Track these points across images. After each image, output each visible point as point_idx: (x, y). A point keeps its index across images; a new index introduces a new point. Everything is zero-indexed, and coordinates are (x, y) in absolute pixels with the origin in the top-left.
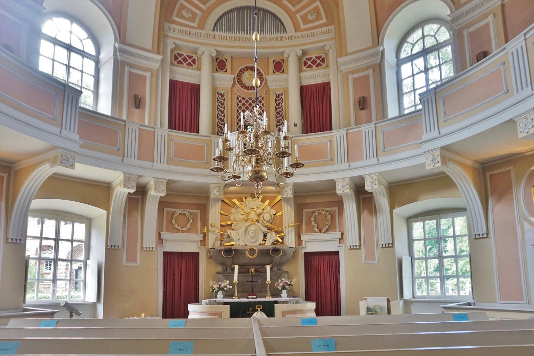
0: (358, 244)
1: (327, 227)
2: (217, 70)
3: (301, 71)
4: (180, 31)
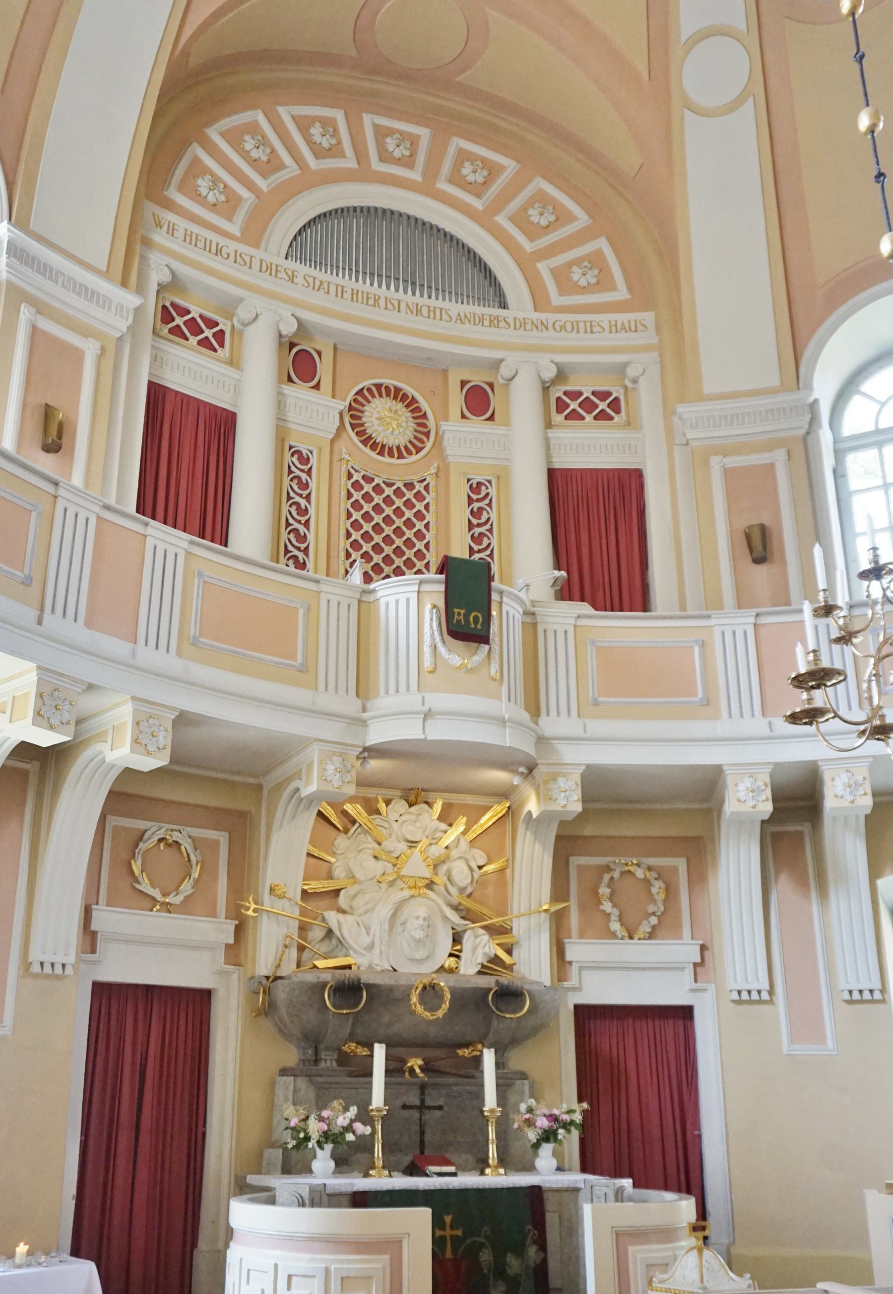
0: (765, 985)
1: (654, 920)
2: (290, 380)
3: (548, 425)
4: (189, 239)
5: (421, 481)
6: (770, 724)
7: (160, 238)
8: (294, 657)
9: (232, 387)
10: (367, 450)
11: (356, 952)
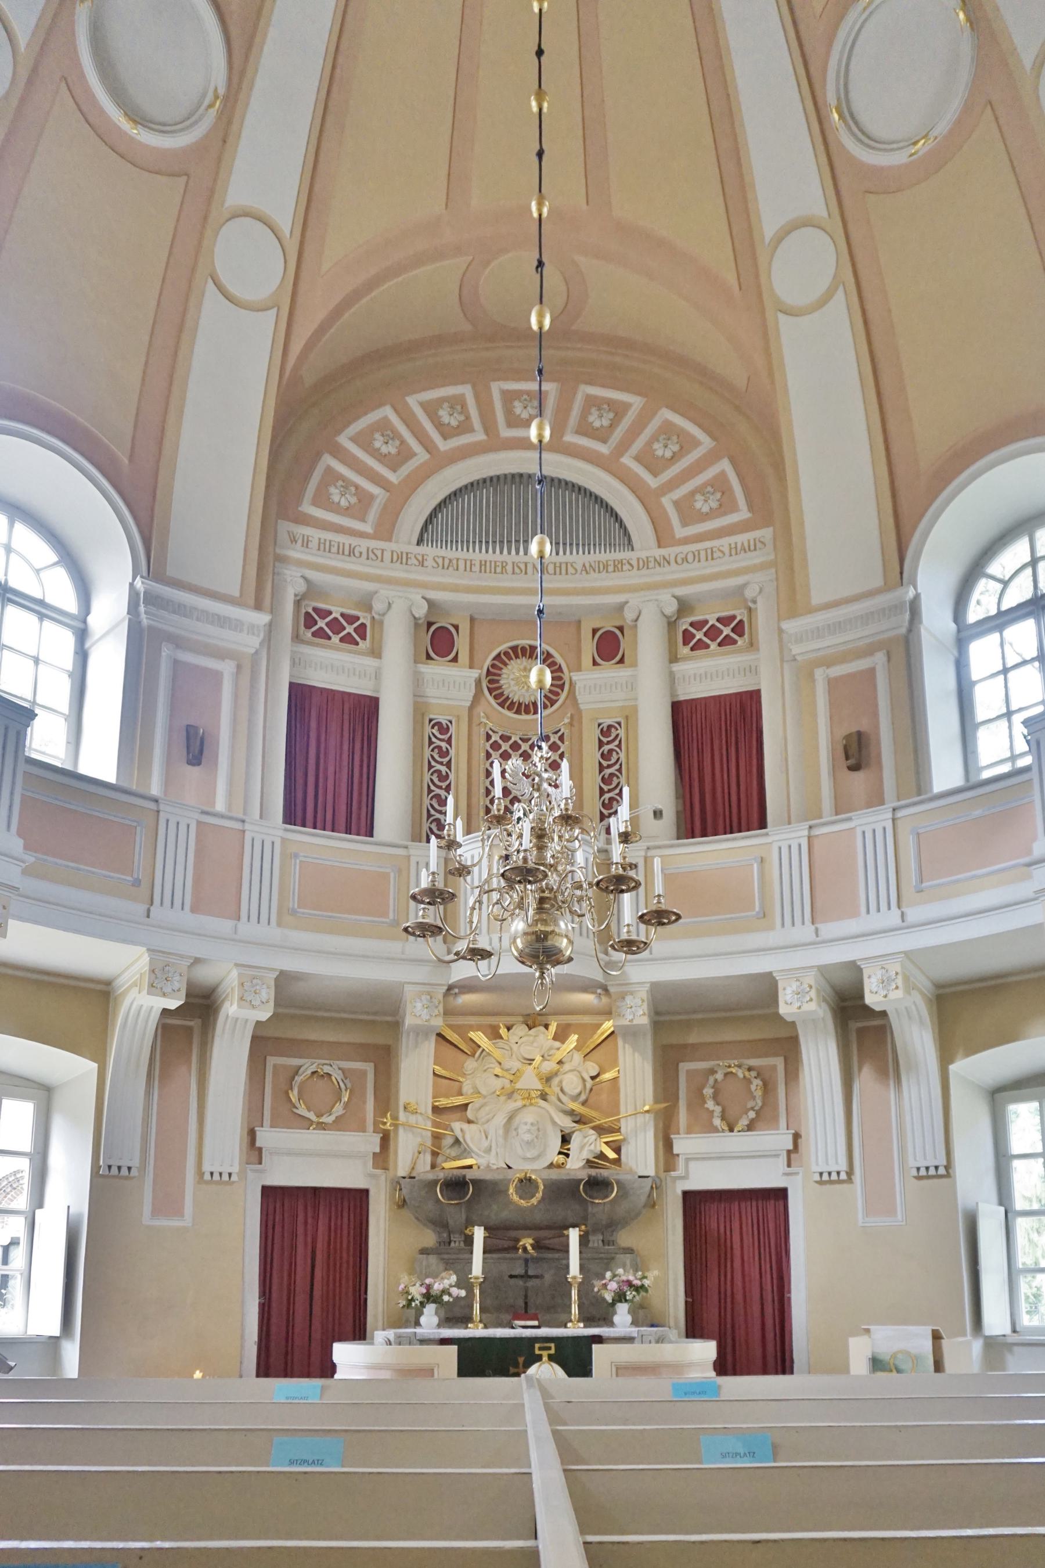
0: (843, 1166)
1: (752, 1114)
3: (674, 658)
4: (324, 547)
5: (556, 733)
6: (817, 930)
7: (295, 553)
8: (385, 914)
9: (373, 676)
10: (506, 712)
11: (478, 1155)
